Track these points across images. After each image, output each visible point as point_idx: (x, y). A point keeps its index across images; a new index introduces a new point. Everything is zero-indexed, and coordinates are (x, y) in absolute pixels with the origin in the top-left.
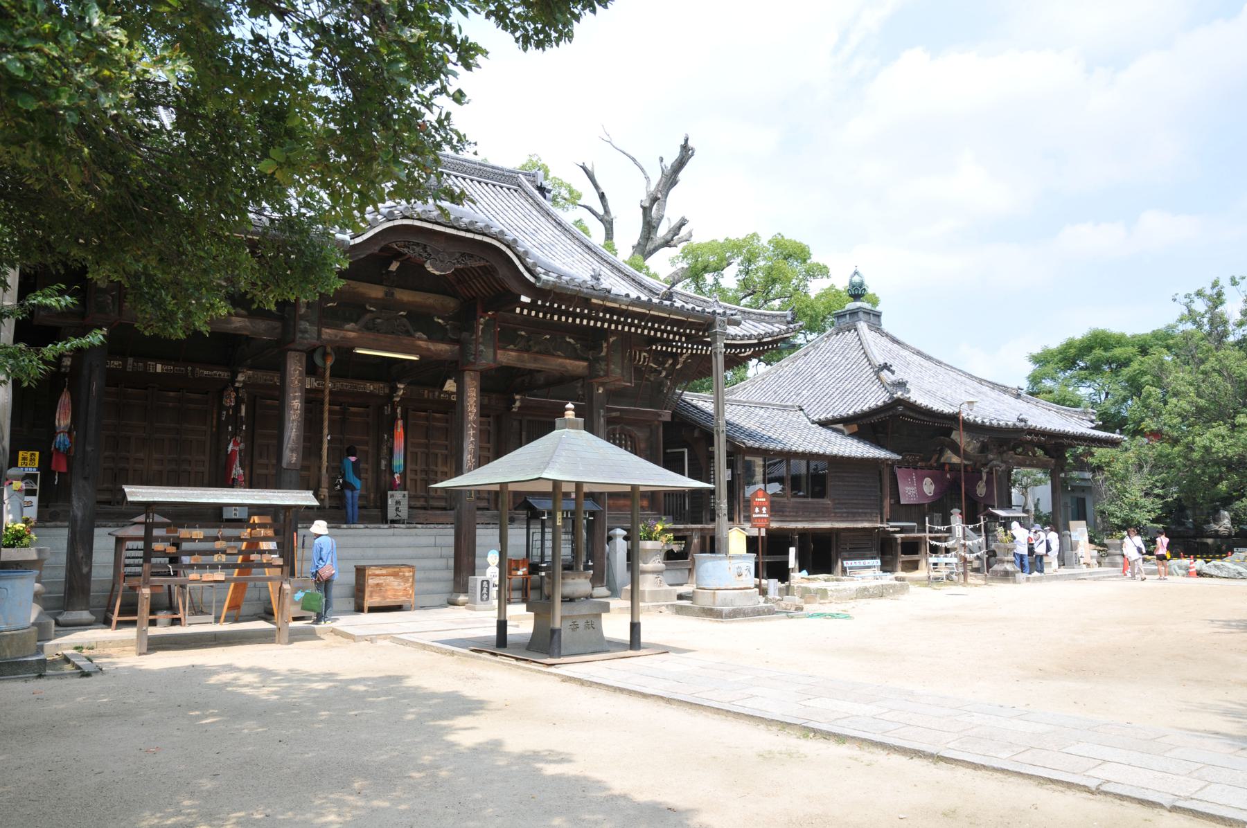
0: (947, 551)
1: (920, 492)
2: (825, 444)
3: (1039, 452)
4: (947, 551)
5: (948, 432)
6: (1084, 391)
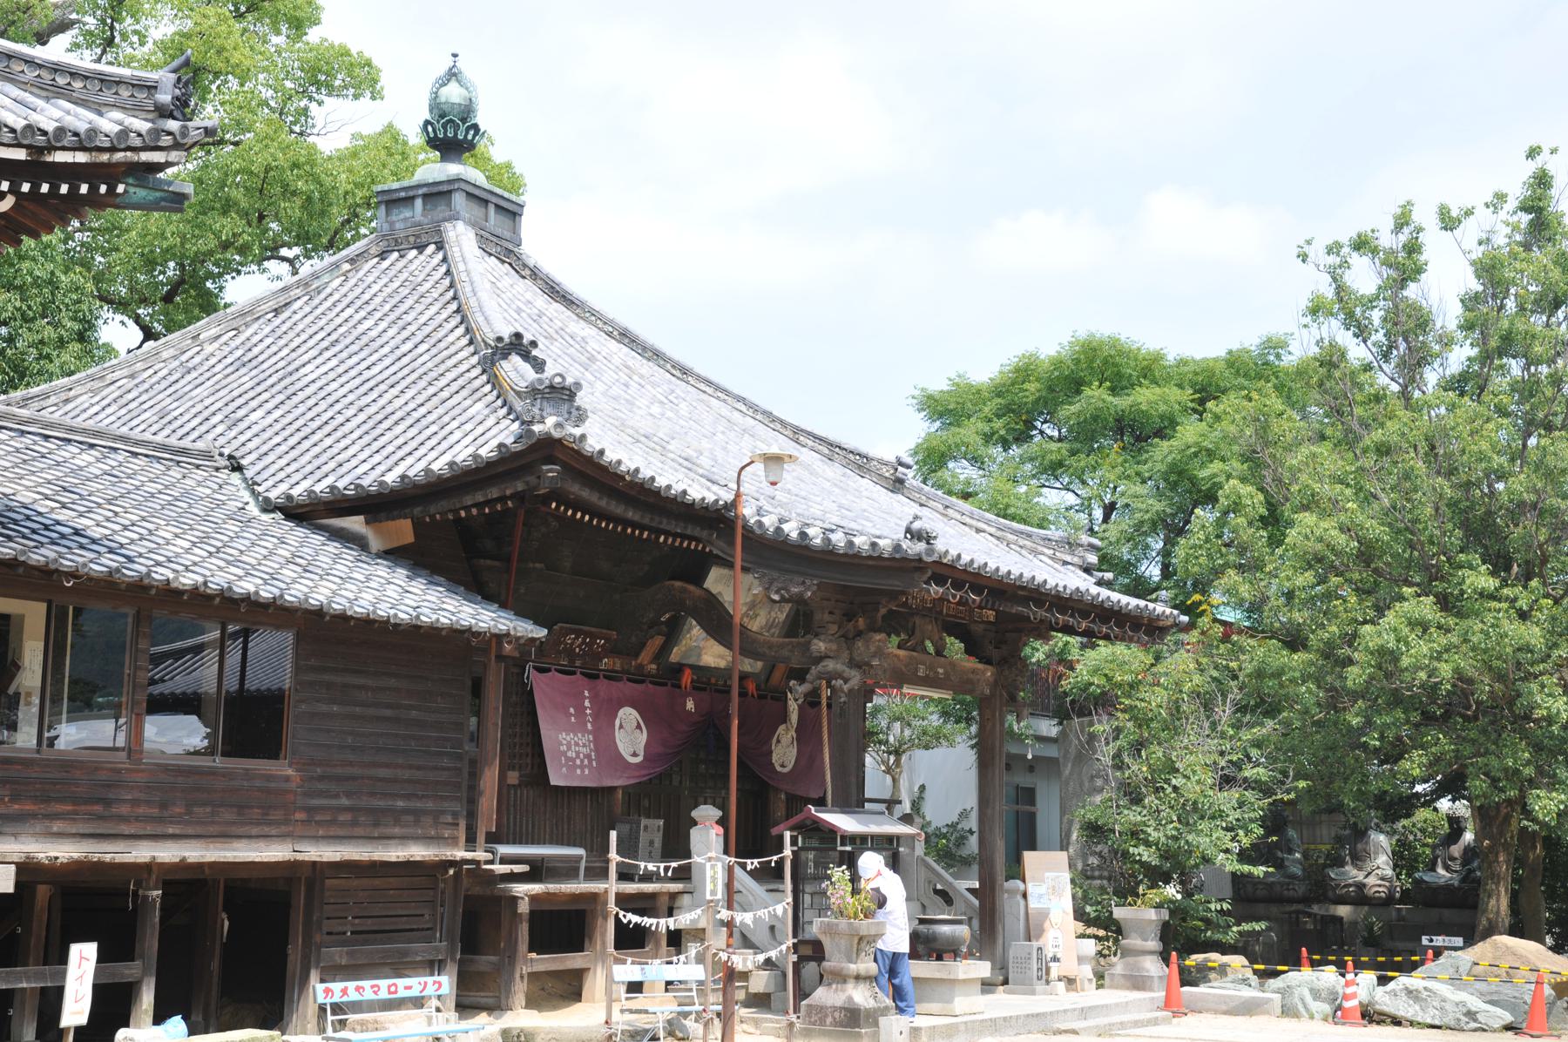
0: (676, 940)
1: (606, 751)
2: (288, 573)
3: (955, 646)
4: (676, 940)
5: (695, 569)
6: (1054, 497)
